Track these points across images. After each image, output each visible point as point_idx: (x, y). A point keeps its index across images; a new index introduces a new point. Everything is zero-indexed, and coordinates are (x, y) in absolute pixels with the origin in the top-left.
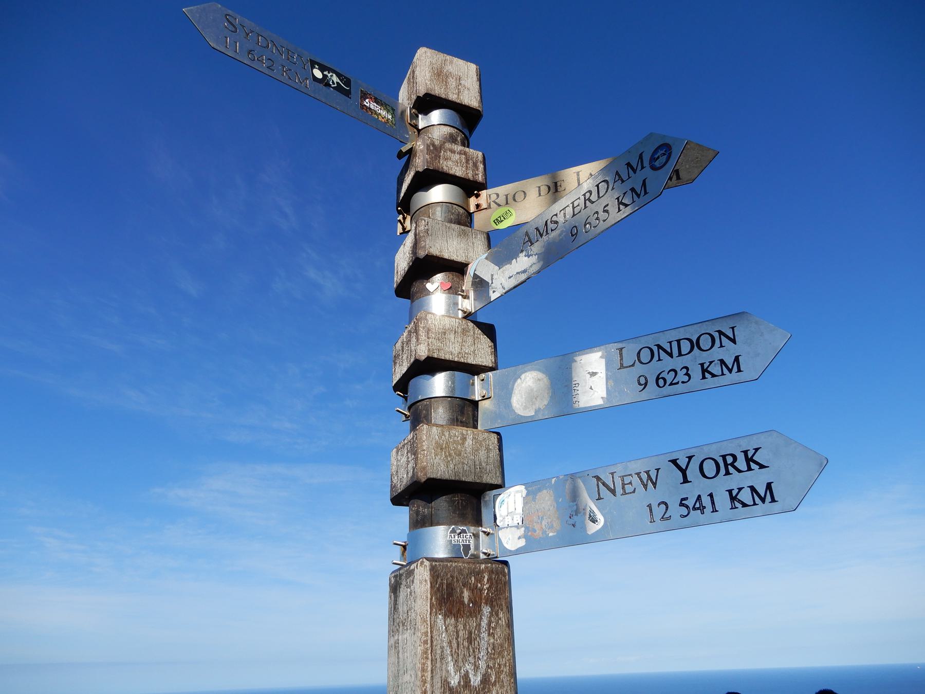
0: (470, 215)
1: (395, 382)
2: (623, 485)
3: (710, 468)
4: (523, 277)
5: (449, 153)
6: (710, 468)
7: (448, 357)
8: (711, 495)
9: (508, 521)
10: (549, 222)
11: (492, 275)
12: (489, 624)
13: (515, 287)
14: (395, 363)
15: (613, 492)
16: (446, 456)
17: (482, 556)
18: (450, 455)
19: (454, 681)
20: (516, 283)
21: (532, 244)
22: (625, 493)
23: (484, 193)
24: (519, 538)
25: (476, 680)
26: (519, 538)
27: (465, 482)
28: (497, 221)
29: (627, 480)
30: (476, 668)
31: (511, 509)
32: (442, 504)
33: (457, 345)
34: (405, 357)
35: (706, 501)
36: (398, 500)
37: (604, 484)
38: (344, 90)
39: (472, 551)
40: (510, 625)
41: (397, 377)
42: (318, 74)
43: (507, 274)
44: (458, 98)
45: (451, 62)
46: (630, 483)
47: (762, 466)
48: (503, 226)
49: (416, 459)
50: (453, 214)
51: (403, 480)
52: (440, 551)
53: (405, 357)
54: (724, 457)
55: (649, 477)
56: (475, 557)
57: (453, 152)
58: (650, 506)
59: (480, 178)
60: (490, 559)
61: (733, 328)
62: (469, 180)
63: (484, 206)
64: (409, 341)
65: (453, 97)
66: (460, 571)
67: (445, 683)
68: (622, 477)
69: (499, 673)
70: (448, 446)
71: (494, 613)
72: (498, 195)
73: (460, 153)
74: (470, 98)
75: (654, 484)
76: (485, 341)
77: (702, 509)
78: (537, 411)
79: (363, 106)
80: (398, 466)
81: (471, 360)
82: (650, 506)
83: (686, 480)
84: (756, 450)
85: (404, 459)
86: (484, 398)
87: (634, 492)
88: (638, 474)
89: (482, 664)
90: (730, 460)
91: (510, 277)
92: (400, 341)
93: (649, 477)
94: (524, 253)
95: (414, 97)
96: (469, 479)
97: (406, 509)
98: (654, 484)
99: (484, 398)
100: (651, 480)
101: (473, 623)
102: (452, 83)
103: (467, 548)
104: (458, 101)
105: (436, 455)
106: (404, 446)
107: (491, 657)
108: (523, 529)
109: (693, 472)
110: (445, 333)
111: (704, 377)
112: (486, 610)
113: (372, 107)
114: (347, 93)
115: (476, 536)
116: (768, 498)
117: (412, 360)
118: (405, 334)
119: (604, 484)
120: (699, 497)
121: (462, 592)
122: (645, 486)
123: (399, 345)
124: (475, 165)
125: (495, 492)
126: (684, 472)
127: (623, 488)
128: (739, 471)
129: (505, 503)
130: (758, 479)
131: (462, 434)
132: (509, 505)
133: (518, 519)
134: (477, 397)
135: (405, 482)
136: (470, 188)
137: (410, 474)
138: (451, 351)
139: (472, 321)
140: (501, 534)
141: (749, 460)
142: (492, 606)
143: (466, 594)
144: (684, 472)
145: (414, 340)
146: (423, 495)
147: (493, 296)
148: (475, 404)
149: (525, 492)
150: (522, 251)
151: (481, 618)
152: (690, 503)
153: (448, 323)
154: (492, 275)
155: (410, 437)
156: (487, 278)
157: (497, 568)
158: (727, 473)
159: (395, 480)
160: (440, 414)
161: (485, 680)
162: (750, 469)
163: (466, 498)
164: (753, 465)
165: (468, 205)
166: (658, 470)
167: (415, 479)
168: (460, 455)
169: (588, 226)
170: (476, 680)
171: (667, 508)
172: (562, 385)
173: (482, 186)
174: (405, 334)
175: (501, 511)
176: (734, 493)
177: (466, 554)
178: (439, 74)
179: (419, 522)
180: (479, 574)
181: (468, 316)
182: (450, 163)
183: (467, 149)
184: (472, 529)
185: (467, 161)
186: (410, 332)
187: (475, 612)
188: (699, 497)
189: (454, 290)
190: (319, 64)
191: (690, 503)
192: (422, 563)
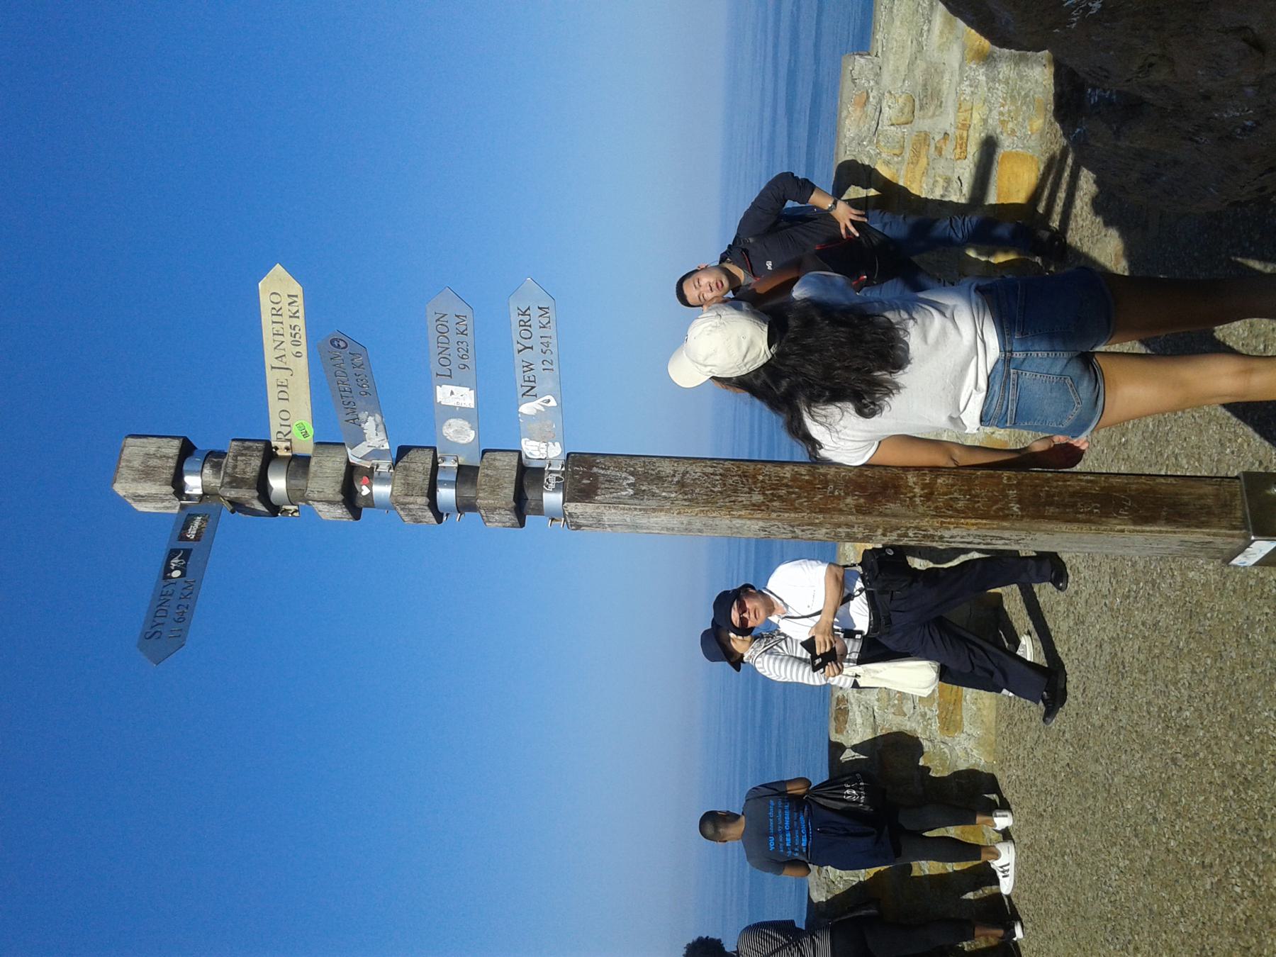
0: (294, 457)
3: (527, 335)
4: (381, 427)
7: (427, 482)
9: (543, 451)
19: (631, 492)
23: (274, 444)
25: (632, 479)
28: (306, 435)
32: (531, 494)
36: (522, 524)
38: (187, 554)
40: (604, 455)
41: (433, 520)
42: (176, 574)
43: (373, 436)
45: (129, 461)
48: (311, 431)
51: (510, 517)
52: (559, 497)
56: (563, 474)
57: (235, 467)
59: (261, 445)
60: (565, 465)
63: (288, 444)
64: (410, 510)
65: (172, 463)
66: (571, 484)
67: (631, 497)
69: (629, 465)
74: (172, 448)
76: (412, 454)
78: (472, 428)
81: (429, 466)
85: (497, 517)
86: (457, 461)
95: (173, 497)
99: (457, 461)
101: (601, 478)
103: (558, 479)
107: (621, 469)
109: (528, 343)
112: (595, 470)
115: (551, 472)
124: (248, 448)
130: (535, 313)
132: (534, 450)
133: (543, 445)
136: (269, 455)
138: (422, 480)
141: (524, 314)
143: (585, 481)
146: (522, 507)
148: (460, 467)
153: (398, 482)
156: (370, 450)
160: (468, 493)
161: (632, 474)
163: (528, 477)
165: (284, 457)
170: (632, 479)
172: (460, 413)
173: (268, 443)
175: (537, 455)
178: (147, 474)
179: (539, 510)
180: (574, 473)
181: (394, 466)
185: (242, 455)
187: (595, 476)
189: (370, 474)
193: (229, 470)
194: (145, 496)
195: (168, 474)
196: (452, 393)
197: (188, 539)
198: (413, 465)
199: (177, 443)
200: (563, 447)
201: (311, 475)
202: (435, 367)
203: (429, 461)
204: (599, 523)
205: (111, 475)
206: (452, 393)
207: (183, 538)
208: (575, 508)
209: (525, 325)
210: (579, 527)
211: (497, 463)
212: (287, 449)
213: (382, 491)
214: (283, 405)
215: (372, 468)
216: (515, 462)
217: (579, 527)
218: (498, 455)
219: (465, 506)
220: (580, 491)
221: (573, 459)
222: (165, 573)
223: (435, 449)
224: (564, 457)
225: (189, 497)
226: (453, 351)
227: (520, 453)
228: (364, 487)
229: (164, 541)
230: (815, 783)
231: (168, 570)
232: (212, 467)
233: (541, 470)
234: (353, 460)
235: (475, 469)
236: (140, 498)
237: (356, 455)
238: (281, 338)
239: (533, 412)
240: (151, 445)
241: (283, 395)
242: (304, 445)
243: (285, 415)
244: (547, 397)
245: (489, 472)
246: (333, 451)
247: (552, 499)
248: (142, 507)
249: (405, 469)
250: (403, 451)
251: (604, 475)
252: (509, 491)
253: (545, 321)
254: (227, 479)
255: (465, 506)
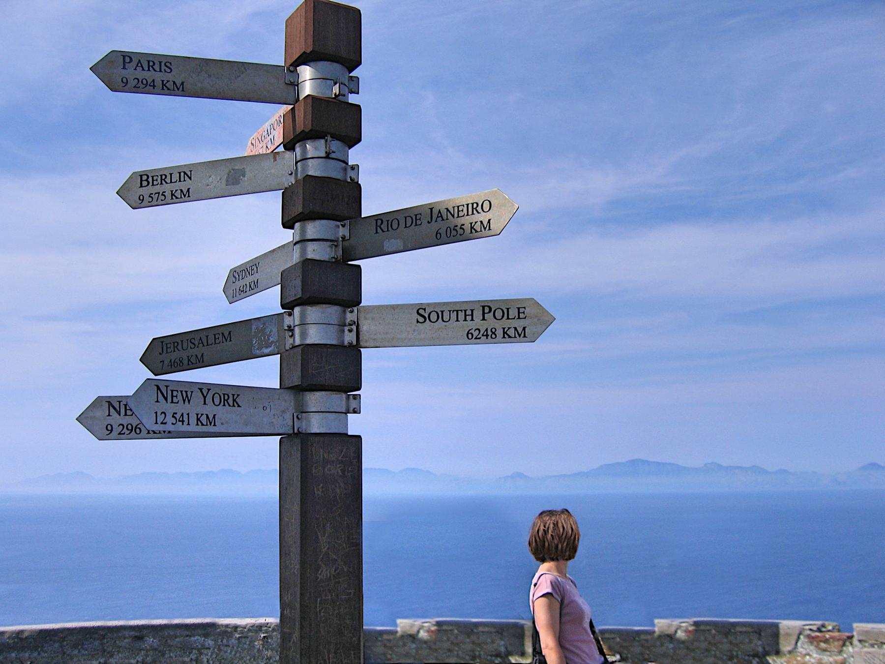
2: (172, 396)
15: (166, 399)
22: (172, 402)
29: (175, 393)
35: (186, 419)
47: (239, 406)
55: (187, 396)
61: (157, 401)
77: (183, 421)
83: (205, 403)
93: (187, 396)
98: (189, 401)
109: (209, 399)
120: (182, 415)
122: (184, 401)
126: (205, 397)
141: (234, 400)
144: (205, 397)
152: (178, 416)
188: (182, 415)
191: (178, 416)
253: (204, 419)
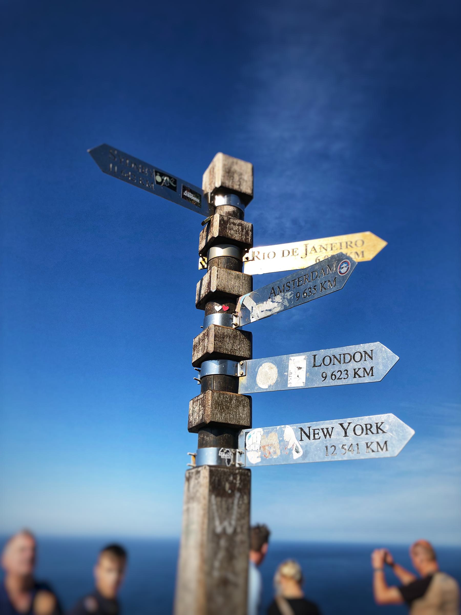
1: (193, 361)
2: (314, 434)
3: (359, 432)
4: (269, 313)
5: (232, 225)
6: (359, 432)
8: (357, 445)
9: (253, 447)
10: (285, 286)
11: (252, 307)
12: (238, 504)
13: (264, 318)
14: (194, 350)
15: (309, 437)
16: (221, 410)
17: (237, 466)
18: (223, 408)
20: (265, 316)
21: (275, 295)
23: (251, 250)
24: (258, 457)
26: (258, 457)
27: (230, 424)
30: (230, 524)
31: (254, 441)
33: (230, 345)
34: (200, 348)
36: (192, 430)
37: (305, 432)
39: (232, 462)
41: (195, 359)
44: (239, 188)
45: (237, 163)
46: (318, 434)
49: (205, 410)
50: (232, 264)
51: (196, 419)
53: (200, 348)
54: (366, 425)
55: (328, 431)
57: (234, 224)
58: (327, 447)
62: (243, 242)
63: (250, 258)
64: (203, 340)
65: (236, 187)
66: (225, 473)
68: (314, 430)
70: (222, 404)
71: (242, 497)
72: (259, 253)
73: (238, 225)
74: (246, 188)
75: (330, 435)
76: (246, 342)
79: (184, 196)
80: (193, 411)
81: (237, 354)
82: (327, 447)
84: (382, 423)
85: (197, 408)
86: (242, 375)
87: (319, 438)
88: (322, 429)
89: (233, 522)
90: (369, 427)
91: (262, 311)
92: (197, 337)
94: (271, 300)
96: (232, 423)
97: (197, 435)
98: (330, 435)
99: (242, 375)
100: (329, 433)
101: (230, 501)
102: (236, 177)
104: (239, 190)
105: (215, 408)
106: (197, 400)
107: (238, 520)
108: (260, 453)
109: (350, 432)
110: (224, 338)
111: (355, 377)
112: (237, 495)
113: (188, 196)
114: (174, 189)
115: (235, 454)
116: (385, 449)
117: (205, 352)
118: (201, 335)
119: (305, 432)
121: (225, 484)
122: (325, 436)
123: (197, 339)
124: (247, 233)
125: (245, 431)
127: (314, 436)
128: (373, 433)
129: (251, 437)
130: (380, 438)
131: (230, 396)
133: (258, 447)
134: (239, 375)
135: (197, 421)
137: (201, 417)
139: (239, 330)
140: (248, 454)
141: (378, 428)
142: (241, 493)
143: (227, 486)
145: (206, 340)
147: (252, 320)
149: (262, 432)
150: (270, 298)
151: (212, 397)
154: (252, 307)
155: (201, 396)
156: (250, 308)
157: (244, 473)
158: (367, 434)
159: (191, 418)
161: (235, 532)
162: (378, 433)
163: (226, 433)
164: (379, 431)
166: (333, 428)
167: (203, 421)
168: (228, 409)
169: (305, 294)
170: (230, 530)
171: (335, 449)
174: (201, 335)
176: (369, 445)
177: (229, 464)
179: (202, 444)
180: (235, 475)
182: (232, 232)
183: (243, 222)
184: (232, 450)
186: (204, 334)
187: (232, 495)
190: (160, 173)
192: (205, 468)
193: (232, 220)
194: (213, 176)
195: (228, 184)
196: (300, 368)
197: (184, 191)
198: (238, 342)
199: (249, 191)
200: (257, 467)
201: (230, 271)
202: (322, 353)
203: (242, 354)
204: (191, 499)
205: (228, 152)
206: (300, 368)
207: (185, 189)
208: (205, 474)
209: (367, 429)
210: (188, 479)
211: (241, 408)
212: (247, 258)
213: (216, 319)
214: (279, 254)
215: (235, 312)
216: (242, 423)
217: (188, 479)
218: (247, 409)
219: (205, 383)
220: (219, 481)
221: (246, 474)
222: (160, 173)
223: (250, 358)
224: (247, 466)
225: (213, 199)
226: (337, 367)
227: (250, 427)
228: (220, 307)
229: (183, 176)
230: (321, 260)
231: (162, 175)
232: (234, 212)
233: (235, 446)
234: (241, 300)
235: (236, 390)
236: (212, 174)
237: (246, 300)
238: (329, 249)
239: (286, 438)
240: (247, 177)
241: (286, 253)
242: (250, 269)
243: (272, 255)
244: (300, 450)
245: (234, 401)
246: (246, 286)
247: (210, 456)
248: (198, 285)
249: (235, 337)
250: (248, 335)
251: (233, 503)
252: (220, 418)
253: (374, 446)
254: (225, 218)
255: (205, 383)
